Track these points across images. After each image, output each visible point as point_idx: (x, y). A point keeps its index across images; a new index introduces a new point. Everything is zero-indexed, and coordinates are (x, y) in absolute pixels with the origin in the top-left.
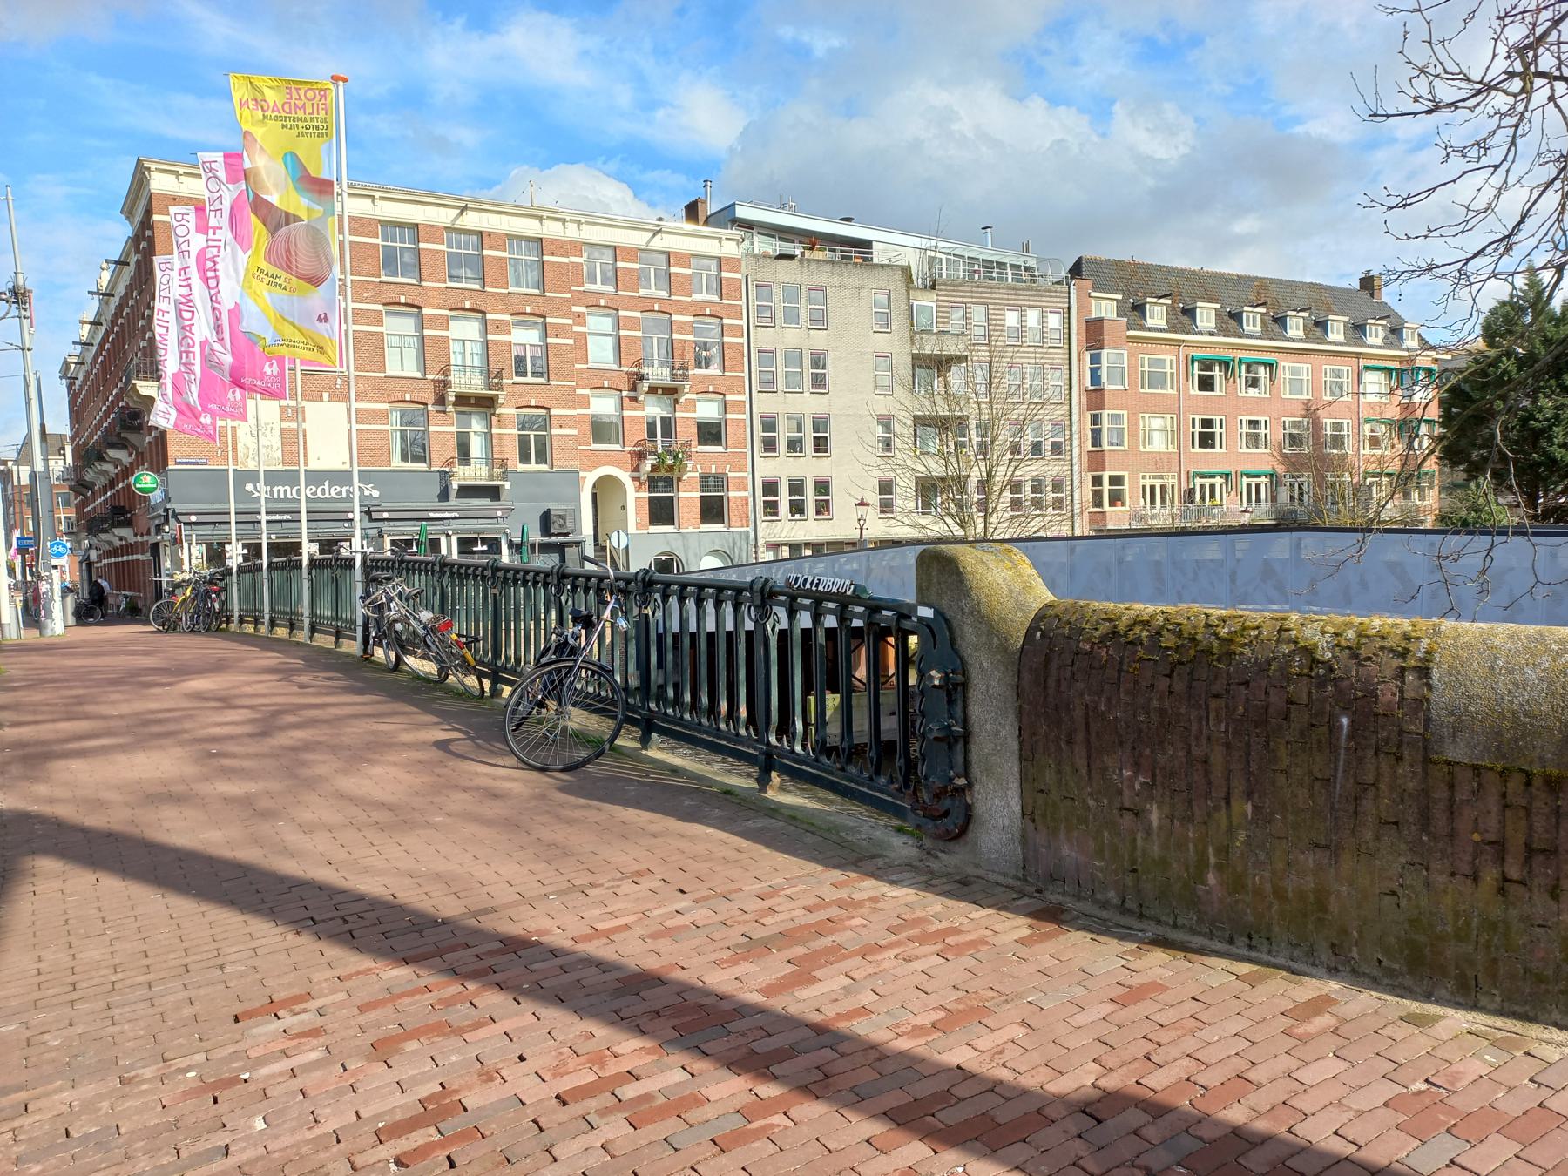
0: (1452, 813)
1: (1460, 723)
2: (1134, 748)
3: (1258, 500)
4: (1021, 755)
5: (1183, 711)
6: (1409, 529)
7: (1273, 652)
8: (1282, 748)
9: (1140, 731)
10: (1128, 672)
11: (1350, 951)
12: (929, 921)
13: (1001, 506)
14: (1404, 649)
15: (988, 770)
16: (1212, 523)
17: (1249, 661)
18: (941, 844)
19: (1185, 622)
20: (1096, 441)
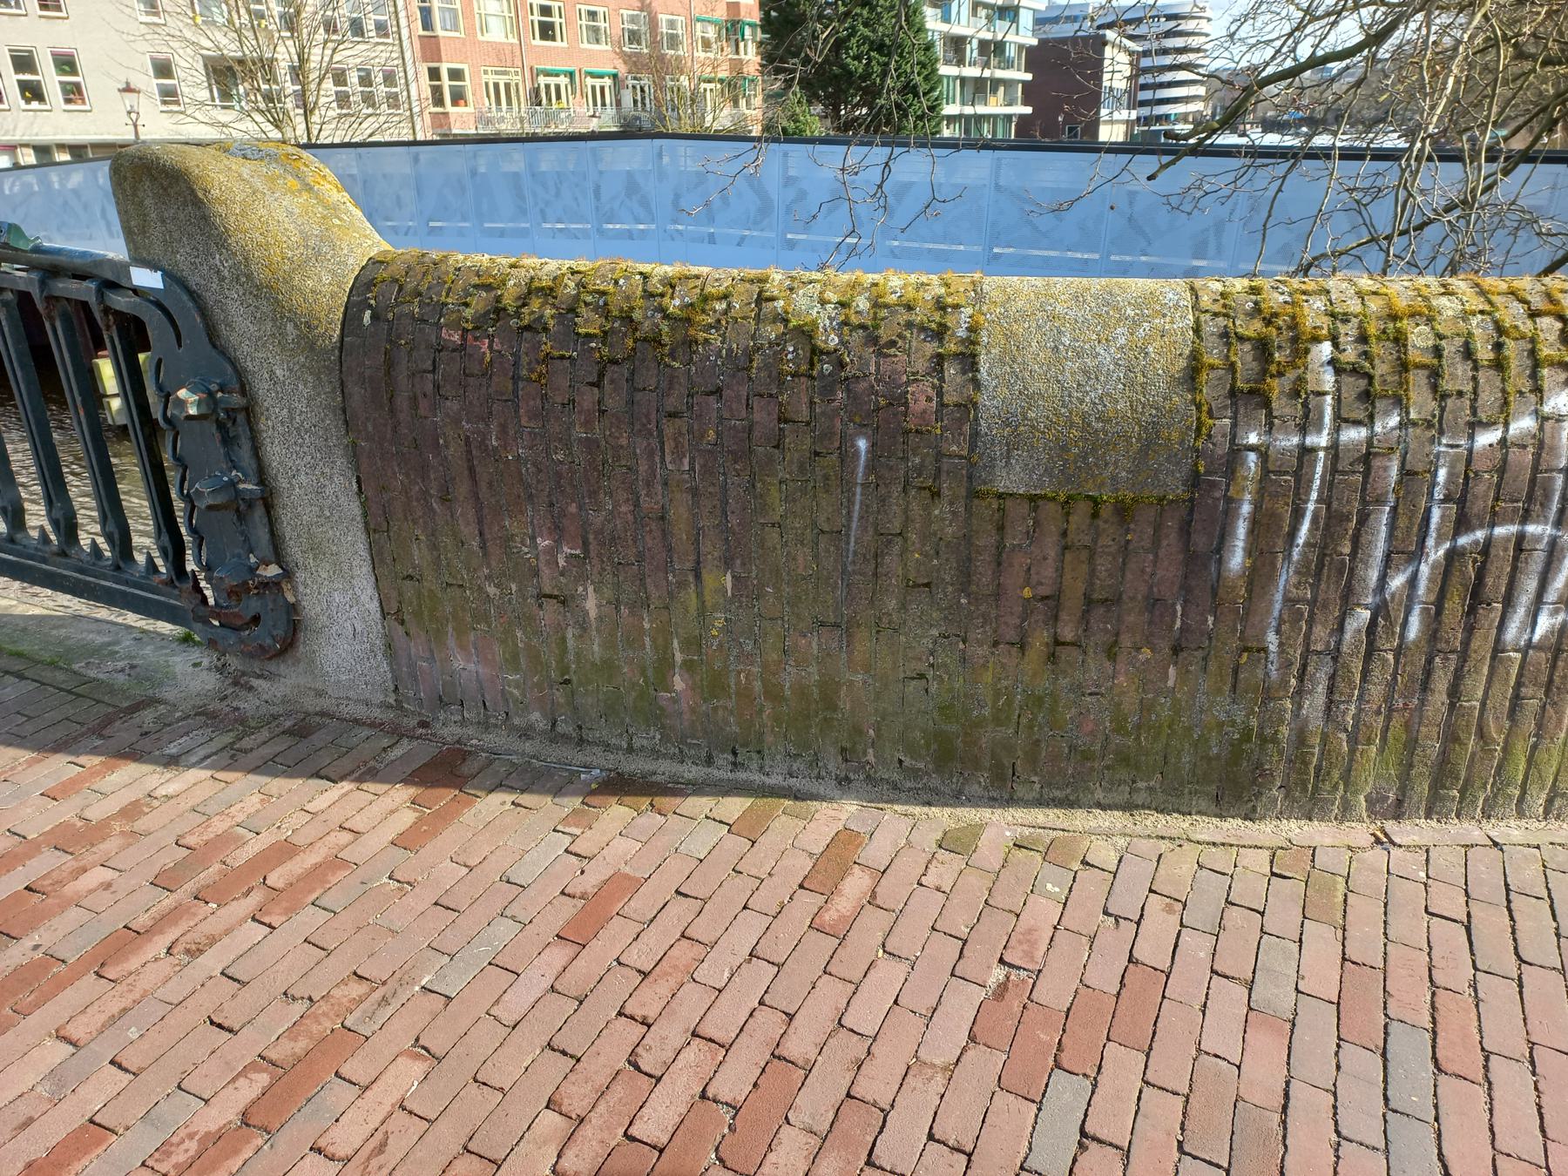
0: (999, 564)
1: (1017, 435)
2: (551, 505)
3: (604, 104)
4: (366, 524)
5: (624, 442)
6: (735, 136)
7: (753, 337)
8: (774, 492)
9: (559, 475)
10: (529, 380)
11: (865, 753)
12: (239, 838)
13: (322, 100)
14: (940, 325)
15: (316, 549)
16: (561, 129)
17: (719, 355)
18: (256, 666)
19: (611, 288)
20: (427, 24)
